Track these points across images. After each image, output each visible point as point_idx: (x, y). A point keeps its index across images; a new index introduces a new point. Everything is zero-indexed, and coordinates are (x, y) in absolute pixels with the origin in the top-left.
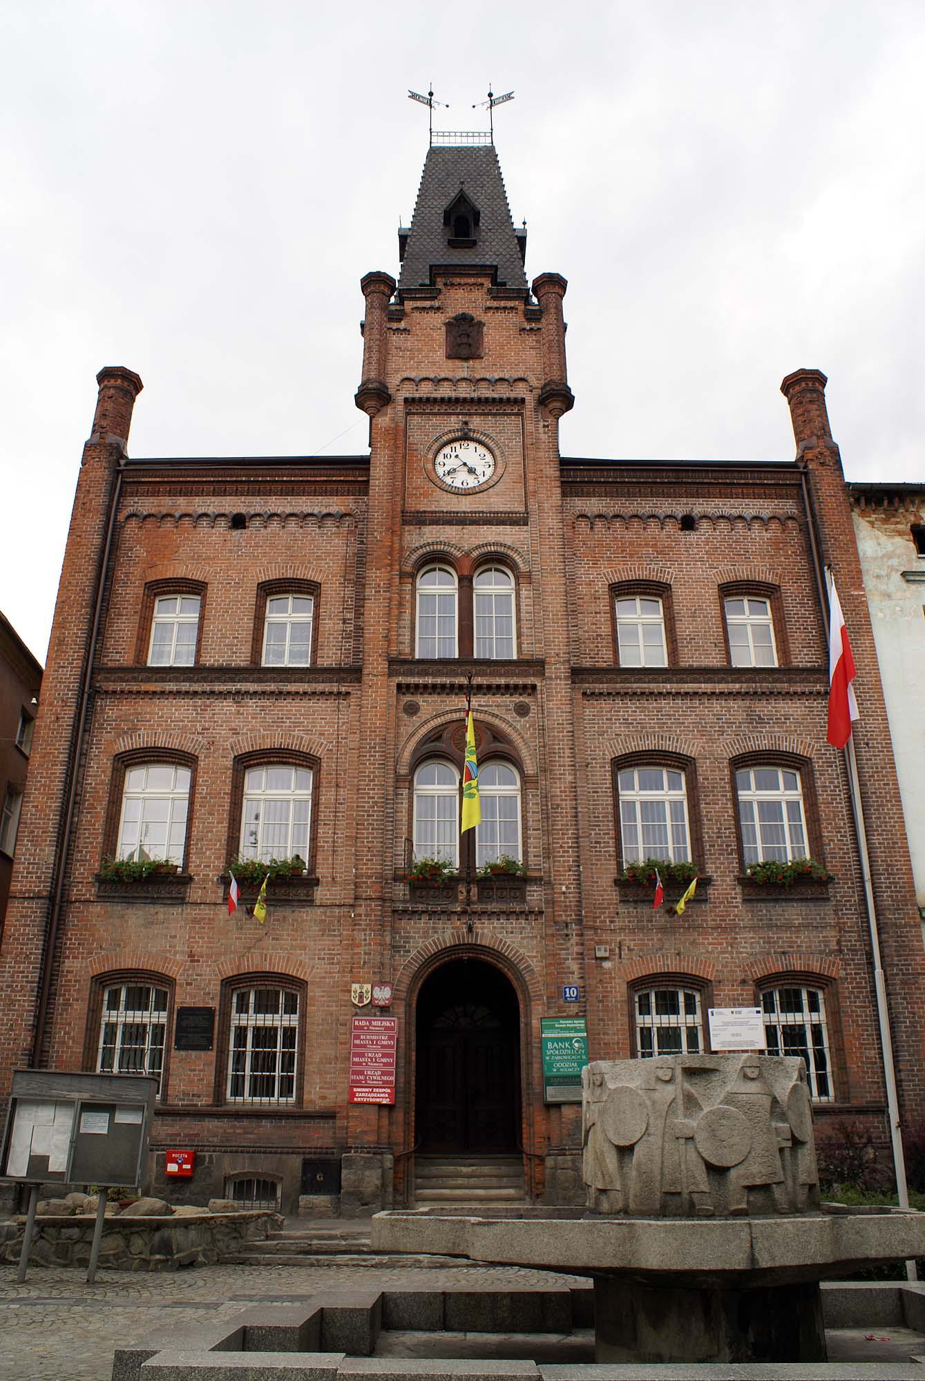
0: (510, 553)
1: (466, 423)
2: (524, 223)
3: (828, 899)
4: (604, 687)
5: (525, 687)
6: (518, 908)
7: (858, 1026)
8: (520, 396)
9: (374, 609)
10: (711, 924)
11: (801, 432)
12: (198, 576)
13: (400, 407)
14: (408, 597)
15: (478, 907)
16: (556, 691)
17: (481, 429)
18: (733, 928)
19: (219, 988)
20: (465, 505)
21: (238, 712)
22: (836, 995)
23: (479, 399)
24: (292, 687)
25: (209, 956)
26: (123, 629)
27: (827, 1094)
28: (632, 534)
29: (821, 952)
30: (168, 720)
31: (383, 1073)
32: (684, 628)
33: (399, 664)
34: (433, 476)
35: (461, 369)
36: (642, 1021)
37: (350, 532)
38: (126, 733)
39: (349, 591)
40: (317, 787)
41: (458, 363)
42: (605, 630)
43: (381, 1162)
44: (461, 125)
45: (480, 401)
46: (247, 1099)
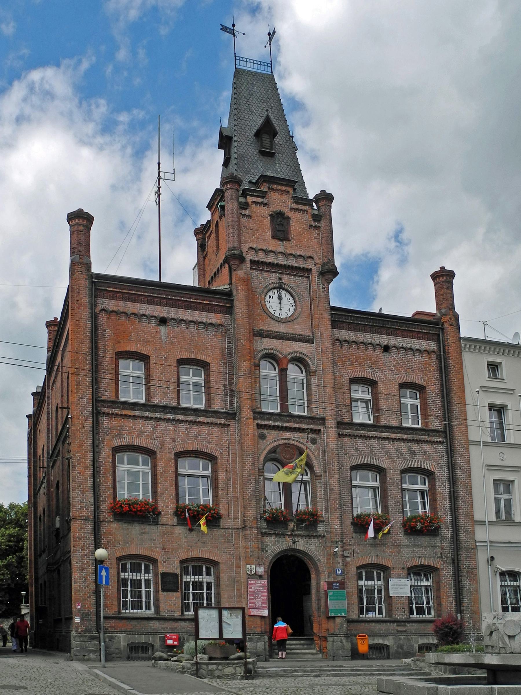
1: (280, 279)
3: (438, 535)
5: (316, 430)
8: (310, 267)
9: (243, 384)
10: (391, 543)
12: (144, 351)
13: (248, 265)
15: (297, 533)
16: (330, 432)
20: (282, 329)
22: (218, 569)
23: (289, 266)
24: (201, 419)
27: (382, 614)
28: (358, 352)
30: (140, 432)
31: (263, 603)
33: (257, 414)
34: (265, 308)
35: (279, 246)
36: (123, 575)
38: (116, 436)
43: (264, 639)
45: (263, 263)
46: (129, 612)
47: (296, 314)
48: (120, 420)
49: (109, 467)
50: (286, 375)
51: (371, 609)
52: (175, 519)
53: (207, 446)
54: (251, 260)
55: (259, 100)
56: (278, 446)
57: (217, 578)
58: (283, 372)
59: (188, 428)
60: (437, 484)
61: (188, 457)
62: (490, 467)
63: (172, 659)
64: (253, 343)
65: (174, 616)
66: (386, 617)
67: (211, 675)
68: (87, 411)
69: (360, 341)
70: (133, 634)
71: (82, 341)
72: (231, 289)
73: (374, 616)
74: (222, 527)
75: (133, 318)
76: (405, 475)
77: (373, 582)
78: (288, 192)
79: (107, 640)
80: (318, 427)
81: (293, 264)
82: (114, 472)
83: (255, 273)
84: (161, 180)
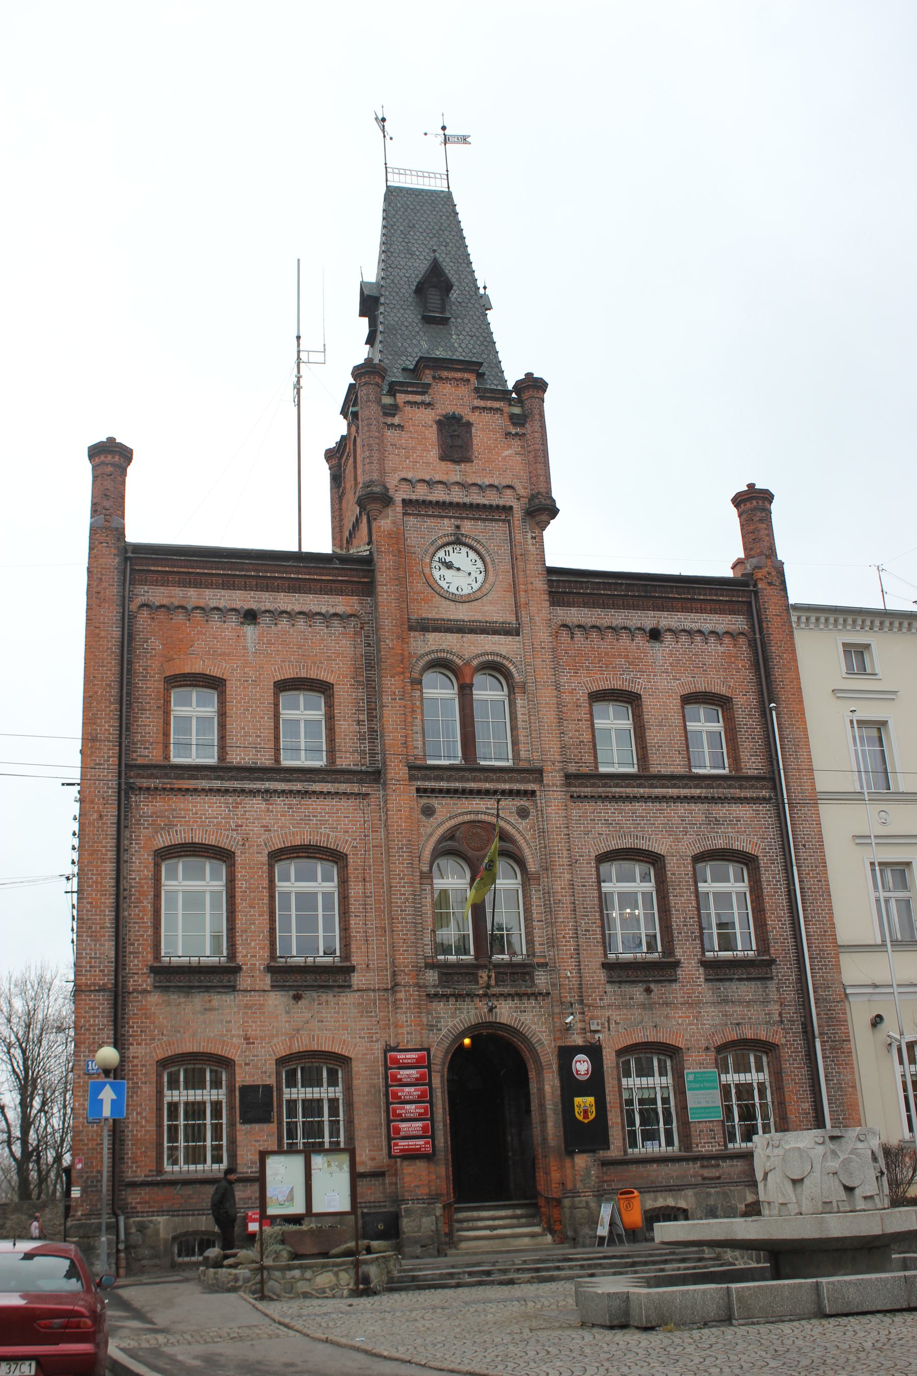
0: (505, 662)
1: (458, 527)
2: (485, 288)
4: (588, 791)
6: (529, 991)
7: (796, 1083)
8: (508, 504)
9: (391, 716)
10: (680, 1000)
11: (751, 549)
12: (216, 672)
13: (399, 509)
14: (418, 703)
17: (472, 534)
18: (698, 1003)
19: (274, 1066)
20: (462, 613)
21: (268, 810)
22: (778, 1059)
23: (471, 504)
24: (317, 787)
25: (263, 1039)
26: (147, 724)
28: (605, 645)
29: (767, 1023)
30: (205, 816)
32: (653, 736)
33: (417, 770)
34: (431, 581)
35: (453, 473)
36: (170, 1096)
37: (356, 633)
38: (162, 829)
39: (361, 693)
40: (343, 882)
41: (451, 466)
42: (587, 737)
44: (421, 168)
47: (487, 586)
48: (169, 799)
49: (148, 887)
50: (472, 694)
51: (650, 1136)
52: (268, 979)
53: (329, 835)
54: (404, 500)
55: (425, 234)
56: (457, 827)
57: (348, 1090)
58: (465, 691)
59: (294, 805)
60: (764, 878)
61: (294, 857)
62: (861, 840)
63: (226, 1262)
64: (407, 643)
65: (247, 1173)
66: (680, 1150)
67: (291, 1292)
68: (108, 788)
69: (606, 625)
70: (183, 1215)
71: (103, 662)
72: (371, 552)
73: (656, 1149)
74: (355, 988)
75: (198, 615)
76: (704, 864)
77: (650, 1079)
78: (469, 380)
79: (133, 1230)
80: (530, 787)
81: (479, 501)
82: (157, 896)
83: (412, 521)
84: (301, 365)
